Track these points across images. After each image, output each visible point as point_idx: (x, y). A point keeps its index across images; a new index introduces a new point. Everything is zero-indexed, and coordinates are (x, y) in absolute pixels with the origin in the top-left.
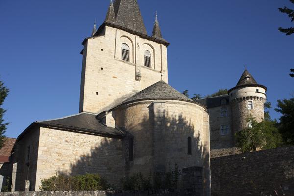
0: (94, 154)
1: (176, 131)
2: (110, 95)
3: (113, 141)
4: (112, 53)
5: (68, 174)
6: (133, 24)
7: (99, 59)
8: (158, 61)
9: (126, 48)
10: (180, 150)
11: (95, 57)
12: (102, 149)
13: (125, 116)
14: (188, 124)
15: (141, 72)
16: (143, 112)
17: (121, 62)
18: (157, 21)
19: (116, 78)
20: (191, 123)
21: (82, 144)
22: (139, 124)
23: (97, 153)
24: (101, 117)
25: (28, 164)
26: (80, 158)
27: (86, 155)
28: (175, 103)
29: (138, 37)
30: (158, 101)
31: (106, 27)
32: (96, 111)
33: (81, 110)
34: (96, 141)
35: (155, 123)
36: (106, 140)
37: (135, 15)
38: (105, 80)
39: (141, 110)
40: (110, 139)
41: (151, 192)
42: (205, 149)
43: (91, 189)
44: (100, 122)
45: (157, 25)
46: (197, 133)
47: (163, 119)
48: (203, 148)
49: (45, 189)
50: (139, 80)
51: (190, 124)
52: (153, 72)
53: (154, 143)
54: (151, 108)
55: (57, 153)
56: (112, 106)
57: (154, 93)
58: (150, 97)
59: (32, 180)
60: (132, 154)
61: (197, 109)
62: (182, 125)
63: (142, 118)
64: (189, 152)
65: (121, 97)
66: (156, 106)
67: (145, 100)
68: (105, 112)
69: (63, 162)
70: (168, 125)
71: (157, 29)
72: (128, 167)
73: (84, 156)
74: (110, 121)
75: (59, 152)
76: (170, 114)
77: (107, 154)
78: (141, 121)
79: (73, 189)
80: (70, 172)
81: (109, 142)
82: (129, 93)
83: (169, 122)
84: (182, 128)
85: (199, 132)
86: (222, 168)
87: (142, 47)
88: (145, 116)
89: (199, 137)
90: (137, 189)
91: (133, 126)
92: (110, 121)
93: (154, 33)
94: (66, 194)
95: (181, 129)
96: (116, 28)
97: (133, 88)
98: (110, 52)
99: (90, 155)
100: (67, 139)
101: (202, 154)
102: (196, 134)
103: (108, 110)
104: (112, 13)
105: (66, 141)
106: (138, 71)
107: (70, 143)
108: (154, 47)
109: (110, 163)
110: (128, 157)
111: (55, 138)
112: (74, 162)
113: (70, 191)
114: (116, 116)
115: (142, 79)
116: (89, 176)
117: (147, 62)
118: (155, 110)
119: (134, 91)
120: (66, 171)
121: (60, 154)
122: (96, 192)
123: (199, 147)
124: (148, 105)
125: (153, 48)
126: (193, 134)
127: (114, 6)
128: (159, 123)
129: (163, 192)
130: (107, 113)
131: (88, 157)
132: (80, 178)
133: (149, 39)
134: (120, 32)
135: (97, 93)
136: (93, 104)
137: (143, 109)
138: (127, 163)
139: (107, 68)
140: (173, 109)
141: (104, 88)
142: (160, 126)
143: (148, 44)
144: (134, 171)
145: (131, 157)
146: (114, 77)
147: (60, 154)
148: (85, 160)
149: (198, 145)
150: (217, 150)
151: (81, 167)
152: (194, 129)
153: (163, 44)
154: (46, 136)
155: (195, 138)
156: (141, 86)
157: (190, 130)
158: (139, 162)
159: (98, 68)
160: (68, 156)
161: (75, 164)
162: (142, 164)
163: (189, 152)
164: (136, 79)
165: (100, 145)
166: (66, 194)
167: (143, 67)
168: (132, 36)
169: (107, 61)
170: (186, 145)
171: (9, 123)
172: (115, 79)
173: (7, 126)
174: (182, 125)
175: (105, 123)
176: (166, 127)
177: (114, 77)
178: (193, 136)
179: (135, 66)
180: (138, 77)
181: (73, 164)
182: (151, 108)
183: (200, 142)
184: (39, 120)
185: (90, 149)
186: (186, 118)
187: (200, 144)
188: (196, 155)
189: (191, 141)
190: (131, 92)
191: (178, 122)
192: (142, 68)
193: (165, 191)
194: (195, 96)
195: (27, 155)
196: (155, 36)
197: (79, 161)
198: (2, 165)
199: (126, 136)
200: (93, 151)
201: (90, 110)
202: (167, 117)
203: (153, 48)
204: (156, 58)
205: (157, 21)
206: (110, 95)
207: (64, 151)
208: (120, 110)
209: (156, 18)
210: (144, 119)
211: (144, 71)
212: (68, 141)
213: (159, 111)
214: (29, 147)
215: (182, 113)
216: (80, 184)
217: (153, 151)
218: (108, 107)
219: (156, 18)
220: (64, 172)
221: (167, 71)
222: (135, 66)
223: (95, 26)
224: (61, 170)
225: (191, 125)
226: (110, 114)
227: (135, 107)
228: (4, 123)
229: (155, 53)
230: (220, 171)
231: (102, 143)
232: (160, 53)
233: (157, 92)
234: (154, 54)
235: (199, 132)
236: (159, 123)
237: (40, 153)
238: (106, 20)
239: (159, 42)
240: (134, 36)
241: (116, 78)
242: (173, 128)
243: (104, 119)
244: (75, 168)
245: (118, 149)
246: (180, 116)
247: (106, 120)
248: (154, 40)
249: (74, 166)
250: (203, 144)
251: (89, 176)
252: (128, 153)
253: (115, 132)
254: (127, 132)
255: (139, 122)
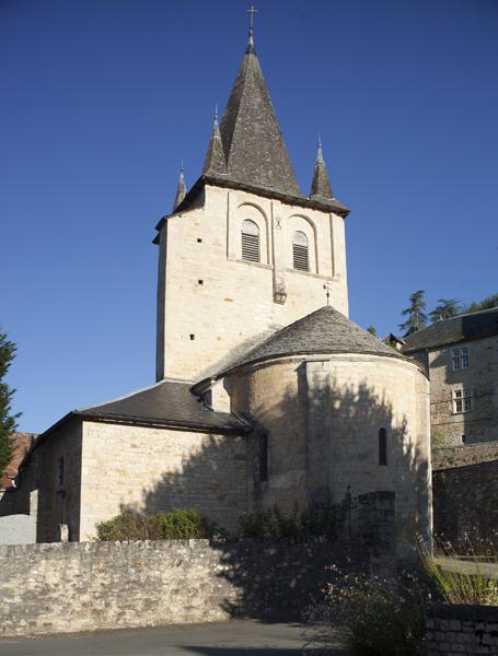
0: (188, 470)
1: (353, 418)
2: (219, 339)
3: (226, 442)
4: (221, 245)
5: (139, 511)
6: (267, 170)
7: (195, 262)
8: (324, 255)
9: (252, 230)
10: (363, 457)
11: (184, 258)
12: (204, 459)
13: (249, 388)
14: (379, 402)
15: (287, 283)
16: (286, 380)
17: (241, 265)
18: (320, 159)
19: (231, 301)
20: (386, 400)
21: (165, 451)
22: (277, 406)
23: (195, 466)
24: (201, 391)
25: (63, 493)
26: (161, 478)
27: (172, 470)
28: (351, 360)
29: (277, 203)
30: (316, 356)
31: (207, 186)
32: (192, 376)
33: (160, 376)
34: (193, 442)
35: (311, 403)
36: (212, 440)
37: (270, 150)
38: (208, 308)
39: (282, 376)
40: (221, 436)
41: (293, 541)
42: (418, 452)
43: (184, 537)
44: (199, 401)
45: (321, 169)
46: (401, 419)
47: (327, 394)
48: (413, 451)
49: (103, 539)
50: (281, 302)
51: (383, 402)
52: (315, 279)
53: (309, 445)
54: (302, 371)
55: (118, 471)
56: (230, 360)
57: (307, 339)
58: (298, 350)
59: (73, 523)
60: (266, 468)
61: (400, 369)
62: (366, 404)
63: (282, 393)
64: (383, 460)
65: (243, 341)
66: (310, 367)
67: (290, 355)
68: (209, 380)
69: (130, 487)
70: (337, 405)
71: (322, 178)
72: (258, 494)
73: (169, 474)
74: (221, 400)
75: (120, 468)
76: (341, 383)
77: (215, 468)
78: (279, 399)
79: (152, 537)
80: (144, 506)
81: (218, 443)
82: (261, 332)
83: (338, 398)
84: (367, 411)
85: (405, 421)
86: (484, 488)
87: (287, 224)
88: (288, 389)
89: (404, 428)
90: (268, 535)
91: (267, 408)
92: (221, 400)
93: (315, 189)
94: (140, 545)
95: (364, 413)
96: (230, 187)
97: (270, 321)
98: (216, 243)
99: (181, 472)
100: (135, 442)
101: (412, 462)
102: (397, 422)
103: (212, 374)
104: (218, 152)
105: (134, 446)
106: (278, 281)
107: (141, 450)
108: (315, 221)
109: (222, 487)
110: (258, 473)
111: (112, 441)
112: (150, 486)
113: (147, 541)
114: (231, 387)
115: (288, 300)
116: (180, 513)
117: (301, 259)
118: (310, 377)
119: (272, 327)
120: (136, 504)
121: (122, 472)
122: (192, 542)
123: (405, 449)
124: (296, 366)
125: (312, 224)
126: (390, 422)
127: (222, 136)
128: (316, 402)
129: (316, 540)
130: (213, 381)
131: (177, 475)
132: (164, 518)
133: (304, 205)
134: (238, 196)
135: (192, 337)
136: (187, 361)
137: (285, 374)
138: (256, 484)
139: (210, 279)
140: (345, 373)
141: (206, 326)
142: (320, 409)
143: (302, 216)
144: (269, 502)
145: (264, 476)
146: (227, 300)
147: (122, 472)
148: (171, 482)
149: (402, 445)
150: (486, 445)
151: (164, 495)
152: (393, 412)
153: (334, 212)
154: (94, 437)
155: (396, 430)
156: (286, 316)
157: (384, 414)
158: (279, 482)
159: (191, 281)
160: (137, 476)
161: (153, 491)
162: (286, 489)
163: (383, 460)
164: (275, 301)
165: (200, 450)
166: (140, 545)
167: (291, 271)
168: (264, 202)
169: (211, 264)
170: (376, 447)
171: (21, 414)
172: (230, 303)
173: (17, 421)
174: (366, 404)
175: (211, 404)
176: (333, 409)
177: (227, 300)
178: (390, 427)
179: (274, 271)
180: (279, 295)
181: (147, 490)
182: (302, 371)
183: (406, 438)
184: (80, 407)
185: (180, 459)
186: (376, 390)
187: (406, 441)
188: (397, 466)
189: (385, 437)
190: (266, 329)
191: (357, 399)
192: (287, 273)
193: (321, 538)
194: (443, 305)
195: (58, 474)
196: (318, 197)
197: (160, 486)
198: (2, 494)
199: (252, 430)
200: (185, 464)
201: (178, 373)
202: (335, 390)
203: (312, 224)
204: (319, 247)
205: (320, 159)
206: (219, 339)
207: (129, 466)
208: (239, 375)
209: (320, 151)
210: (286, 395)
211: (294, 281)
212: (138, 444)
213: (316, 378)
214: (62, 460)
215: (366, 378)
216: (164, 528)
217: (307, 460)
218: (215, 366)
219: (320, 151)
220: (132, 507)
221: (345, 275)
222: (274, 271)
223: (182, 176)
224: (126, 502)
225: (386, 404)
226: (221, 381)
227: (269, 370)
228: (11, 414)
229: (318, 235)
230: (480, 497)
231: (203, 446)
232: (328, 234)
233: (315, 336)
234: (316, 239)
235: (405, 416)
236: (316, 402)
237: (85, 471)
238: (205, 170)
239: (326, 209)
240: (269, 201)
241: (231, 301)
242: (348, 412)
243: (207, 395)
244: (153, 499)
245: (238, 457)
246: (362, 387)
247: (211, 397)
248: (315, 206)
249: (151, 493)
250: (414, 441)
251: (180, 513)
252: (258, 465)
253: (230, 424)
254: (255, 423)
255: (277, 401)
